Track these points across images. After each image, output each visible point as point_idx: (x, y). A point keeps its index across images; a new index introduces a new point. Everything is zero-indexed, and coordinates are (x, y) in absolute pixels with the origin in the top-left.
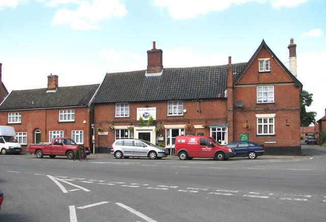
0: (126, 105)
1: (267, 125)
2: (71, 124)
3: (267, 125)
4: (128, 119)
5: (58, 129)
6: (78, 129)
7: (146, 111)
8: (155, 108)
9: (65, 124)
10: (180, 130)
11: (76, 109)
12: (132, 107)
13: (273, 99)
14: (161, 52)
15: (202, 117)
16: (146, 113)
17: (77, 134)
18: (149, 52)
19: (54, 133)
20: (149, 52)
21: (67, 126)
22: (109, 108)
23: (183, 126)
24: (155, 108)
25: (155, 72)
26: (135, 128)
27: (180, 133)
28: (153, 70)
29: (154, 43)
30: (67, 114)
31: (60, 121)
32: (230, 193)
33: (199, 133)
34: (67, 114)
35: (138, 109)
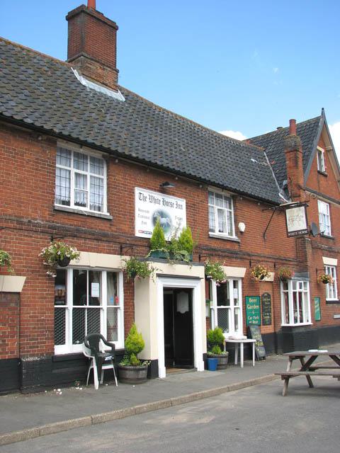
7: (161, 207)
13: (217, 234)
15: (267, 252)
16: (162, 214)
18: (71, 17)
22: (30, 152)
23: (240, 272)
24: (183, 202)
26: (158, 267)
35: (137, 190)
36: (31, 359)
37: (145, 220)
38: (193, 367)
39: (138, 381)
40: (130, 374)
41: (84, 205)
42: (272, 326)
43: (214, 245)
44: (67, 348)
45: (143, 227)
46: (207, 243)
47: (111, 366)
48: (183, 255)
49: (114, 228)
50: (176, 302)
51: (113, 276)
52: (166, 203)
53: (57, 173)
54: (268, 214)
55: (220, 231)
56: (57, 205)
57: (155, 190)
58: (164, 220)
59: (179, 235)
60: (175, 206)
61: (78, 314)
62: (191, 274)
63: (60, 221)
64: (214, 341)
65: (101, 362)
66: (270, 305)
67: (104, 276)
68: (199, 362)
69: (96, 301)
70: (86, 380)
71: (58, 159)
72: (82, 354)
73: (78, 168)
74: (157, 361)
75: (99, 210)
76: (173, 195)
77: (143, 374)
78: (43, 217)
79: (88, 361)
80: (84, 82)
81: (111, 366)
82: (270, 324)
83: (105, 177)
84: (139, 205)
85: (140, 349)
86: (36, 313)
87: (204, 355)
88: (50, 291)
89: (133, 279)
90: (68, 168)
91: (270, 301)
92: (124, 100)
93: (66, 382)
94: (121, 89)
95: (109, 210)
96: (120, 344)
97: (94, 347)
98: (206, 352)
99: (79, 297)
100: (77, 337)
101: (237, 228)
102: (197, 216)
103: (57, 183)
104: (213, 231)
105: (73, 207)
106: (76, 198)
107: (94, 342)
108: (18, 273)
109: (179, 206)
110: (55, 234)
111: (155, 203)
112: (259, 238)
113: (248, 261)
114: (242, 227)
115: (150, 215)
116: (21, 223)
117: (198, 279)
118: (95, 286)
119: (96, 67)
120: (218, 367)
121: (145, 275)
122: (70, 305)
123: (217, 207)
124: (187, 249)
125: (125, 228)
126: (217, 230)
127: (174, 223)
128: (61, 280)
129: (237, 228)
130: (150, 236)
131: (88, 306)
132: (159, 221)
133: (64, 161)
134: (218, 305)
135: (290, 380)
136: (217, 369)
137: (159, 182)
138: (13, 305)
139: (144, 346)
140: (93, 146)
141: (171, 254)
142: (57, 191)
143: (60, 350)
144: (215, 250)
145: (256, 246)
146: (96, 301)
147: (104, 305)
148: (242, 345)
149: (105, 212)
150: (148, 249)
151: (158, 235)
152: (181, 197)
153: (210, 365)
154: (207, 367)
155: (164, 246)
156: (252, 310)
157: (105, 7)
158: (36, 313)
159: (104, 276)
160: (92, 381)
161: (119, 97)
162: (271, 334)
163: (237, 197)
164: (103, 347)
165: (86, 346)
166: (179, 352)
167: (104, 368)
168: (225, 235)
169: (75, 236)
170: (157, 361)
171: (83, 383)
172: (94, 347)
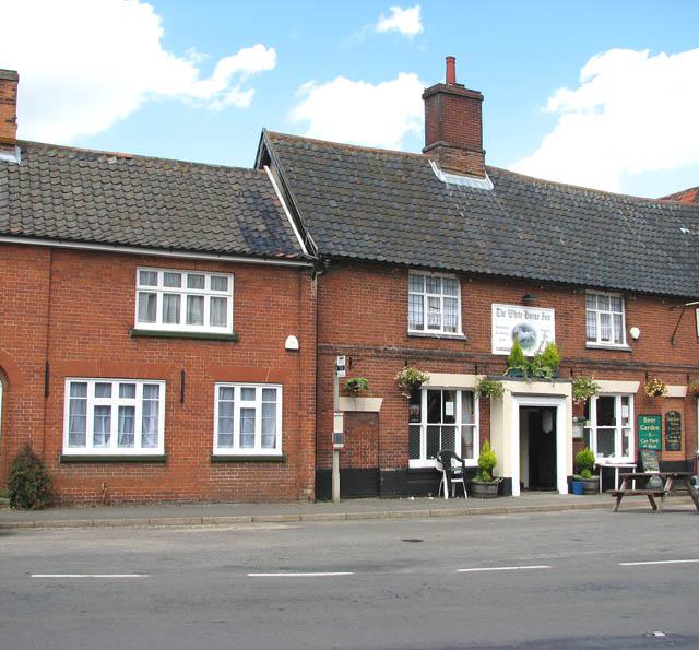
0: (446, 287)
1: (108, 408)
2: (213, 348)
3: (108, 408)
4: (459, 347)
5: (127, 371)
6: (249, 375)
7: (523, 321)
8: (551, 313)
9: (175, 344)
10: (618, 402)
11: (244, 275)
12: (474, 296)
13: (599, 343)
14: (476, 99)
15: (677, 360)
16: (524, 329)
17: (248, 404)
18: (428, 96)
19: (103, 389)
20: (669, 55)
21: (190, 353)
22: (382, 286)
23: (631, 387)
24: (551, 313)
25: (468, 173)
26: (510, 386)
27: (620, 411)
28: (462, 164)
29: (451, 61)
30: (184, 290)
31: (141, 326)
32: (542, 562)
33: (668, 414)
34: (184, 290)
35: (494, 307)
36: (387, 469)
37: (503, 337)
38: (556, 489)
39: (487, 496)
40: (479, 489)
41: (438, 328)
42: (683, 451)
43: (592, 356)
44: (422, 462)
45: (501, 344)
46: (584, 355)
47: (461, 480)
48: (545, 373)
49: (468, 348)
50: (537, 428)
51: (468, 395)
52: (527, 315)
53: (410, 299)
54: (677, 312)
55: (603, 340)
56: (411, 331)
57: (516, 303)
58: (525, 335)
59: (543, 349)
60: (540, 317)
61: (432, 432)
62: (559, 394)
63: (413, 346)
64: (581, 465)
65: (451, 475)
66: (679, 426)
67: (459, 396)
68: (562, 485)
69: (451, 419)
70: (438, 492)
71: (410, 286)
72: (435, 469)
73: (431, 292)
74: (510, 479)
75: (454, 331)
76: (539, 306)
77: (494, 489)
78: (397, 344)
79: (441, 474)
80: (443, 177)
81: (461, 480)
82: (679, 450)
83: (459, 297)
84: (496, 321)
85: (492, 466)
86: (395, 428)
87: (569, 478)
88: (404, 412)
89: (486, 399)
90: (421, 294)
91: (680, 422)
92: (492, 187)
93: (420, 492)
94: (490, 170)
95: (463, 330)
96: (472, 462)
97: (446, 463)
98: (571, 474)
99: (434, 415)
100: (431, 454)
101: (629, 334)
102: (570, 327)
103: (410, 309)
104: (594, 340)
105: (427, 331)
106: (429, 321)
107: (446, 458)
108: (376, 395)
109: (545, 317)
110: (409, 358)
111: (516, 317)
112: (665, 343)
113: (643, 374)
114: (635, 332)
115: (510, 331)
116: (377, 351)
117: (563, 396)
118: (449, 405)
119: (458, 156)
120: (584, 492)
121: (499, 394)
122: (424, 423)
123: (599, 312)
124: (550, 365)
125: (481, 346)
126: (599, 339)
127: (539, 339)
128: (416, 400)
129: (629, 334)
130: (509, 353)
131: (442, 424)
132: (522, 338)
133: (416, 286)
134: (599, 424)
135: (623, 498)
136: (583, 494)
137: (521, 294)
138: (372, 422)
139: (495, 463)
140: (444, 270)
141: (530, 371)
142: (410, 317)
143: (414, 464)
144: (590, 362)
145: (659, 354)
146: (451, 419)
147: (459, 423)
148: (617, 471)
149: (460, 333)
150: (506, 366)
151: (516, 352)
152: (549, 307)
153: (575, 488)
154: (571, 491)
155: (522, 364)
156: (647, 432)
157: (467, 79)
158: (395, 428)
159: (459, 396)
160: (442, 494)
161: (486, 184)
162: (681, 462)
163: (632, 298)
164: (455, 464)
165: (438, 460)
166: (540, 471)
167: (453, 480)
168: (611, 344)
169: (429, 359)
170: (510, 479)
171: (435, 495)
172: (446, 463)
